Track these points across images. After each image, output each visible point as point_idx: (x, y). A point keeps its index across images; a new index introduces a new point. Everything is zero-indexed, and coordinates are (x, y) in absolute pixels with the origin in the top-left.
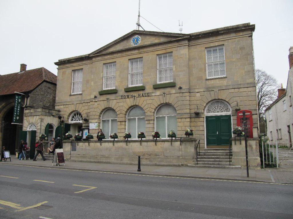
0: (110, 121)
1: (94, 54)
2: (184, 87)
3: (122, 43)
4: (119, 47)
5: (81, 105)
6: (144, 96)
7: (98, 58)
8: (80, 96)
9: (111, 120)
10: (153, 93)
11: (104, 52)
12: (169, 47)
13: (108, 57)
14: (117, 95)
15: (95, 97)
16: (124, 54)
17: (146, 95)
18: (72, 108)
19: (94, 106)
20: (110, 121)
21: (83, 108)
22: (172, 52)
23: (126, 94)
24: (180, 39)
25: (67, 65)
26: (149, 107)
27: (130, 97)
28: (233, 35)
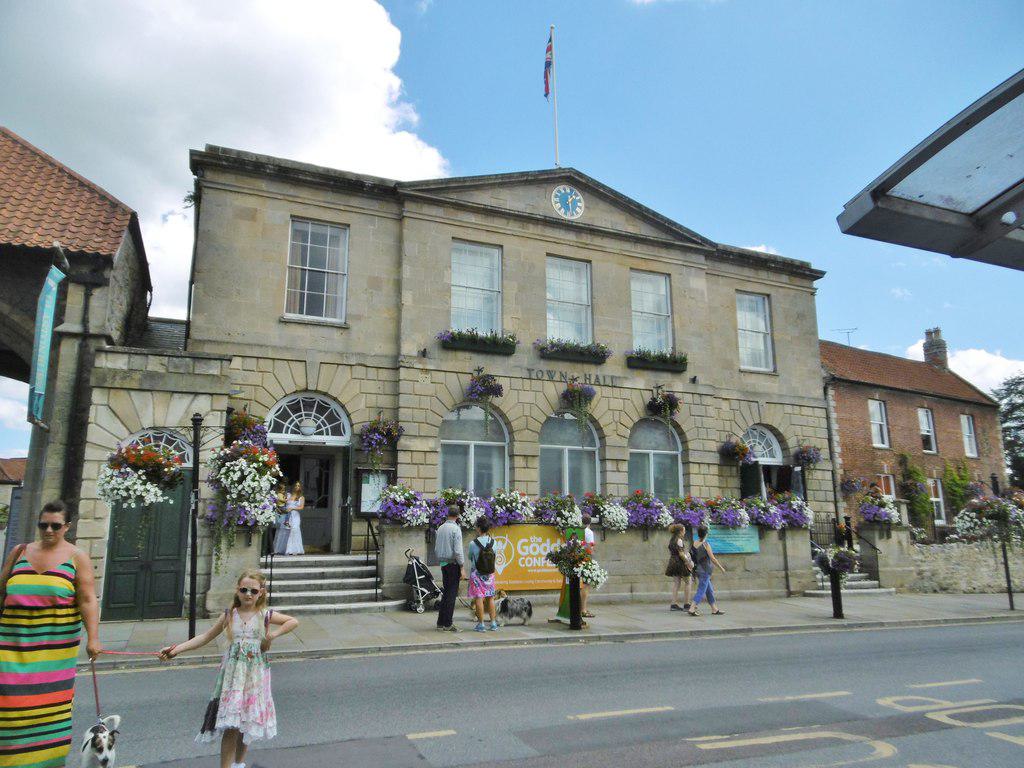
0: (472, 451)
1: (419, 190)
2: (701, 379)
3: (520, 191)
4: (509, 200)
5: (344, 374)
6: (599, 385)
7: (427, 210)
8: (336, 334)
9: (570, 451)
10: (626, 378)
11: (454, 197)
12: (442, 221)
13: (472, 218)
14: (511, 361)
15: (424, 354)
16: (532, 229)
17: (608, 382)
18: (288, 381)
19: (417, 385)
20: (472, 451)
21: (356, 387)
22: (349, 226)
23: (544, 366)
24: (691, 248)
25: (263, 185)
26: (617, 419)
27: (557, 377)
28: (784, 278)
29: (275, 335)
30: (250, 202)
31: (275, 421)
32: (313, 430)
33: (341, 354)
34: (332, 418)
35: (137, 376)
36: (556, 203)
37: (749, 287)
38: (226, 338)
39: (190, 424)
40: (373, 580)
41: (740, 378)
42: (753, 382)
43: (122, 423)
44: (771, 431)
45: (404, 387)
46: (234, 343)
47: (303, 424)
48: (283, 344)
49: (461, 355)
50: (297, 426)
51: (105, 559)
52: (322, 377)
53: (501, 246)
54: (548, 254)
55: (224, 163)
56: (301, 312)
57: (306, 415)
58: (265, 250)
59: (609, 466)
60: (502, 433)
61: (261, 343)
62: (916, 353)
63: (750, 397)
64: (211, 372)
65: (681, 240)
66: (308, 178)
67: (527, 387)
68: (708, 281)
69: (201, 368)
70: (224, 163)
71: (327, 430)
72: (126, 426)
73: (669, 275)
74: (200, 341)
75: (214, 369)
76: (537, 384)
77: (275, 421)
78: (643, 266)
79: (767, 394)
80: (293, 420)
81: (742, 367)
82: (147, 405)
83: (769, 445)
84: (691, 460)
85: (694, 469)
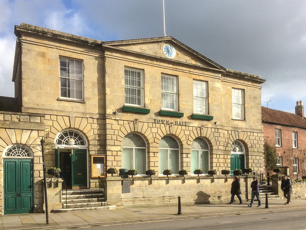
5: (85, 121)
14: (147, 116)
15: (115, 113)
18: (63, 124)
23: (160, 118)
29: (56, 105)
30: (43, 49)
31: (83, 139)
32: (74, 143)
33: (83, 113)
34: (80, 138)
35: (8, 123)
36: (165, 51)
37: (237, 86)
38: (37, 107)
39: (40, 143)
40: (103, 198)
41: (232, 122)
42: (237, 123)
43: (4, 141)
44: (242, 142)
45: (108, 126)
46: (40, 109)
47: (69, 140)
48: (60, 109)
49: (129, 114)
50: (67, 141)
51: (3, 193)
52: (76, 123)
53: (207, 82)
54: (194, 79)
55: (30, 32)
56: (130, 103)
57: (70, 137)
58: (49, 70)
59: (184, 155)
60: (145, 144)
61: (52, 109)
62: (293, 111)
63: (236, 129)
64: (37, 121)
65: (212, 67)
66: (66, 39)
67: (154, 126)
68: (222, 84)
69: (33, 120)
70: (30, 32)
71: (79, 143)
72: (5, 143)
73: (207, 82)
74: (27, 108)
75: (38, 120)
76: (158, 125)
77: (83, 139)
78: (198, 78)
79: (242, 128)
80: (65, 139)
81: (233, 118)
82: (13, 135)
83: (241, 147)
84: (150, 151)
85: (214, 156)
